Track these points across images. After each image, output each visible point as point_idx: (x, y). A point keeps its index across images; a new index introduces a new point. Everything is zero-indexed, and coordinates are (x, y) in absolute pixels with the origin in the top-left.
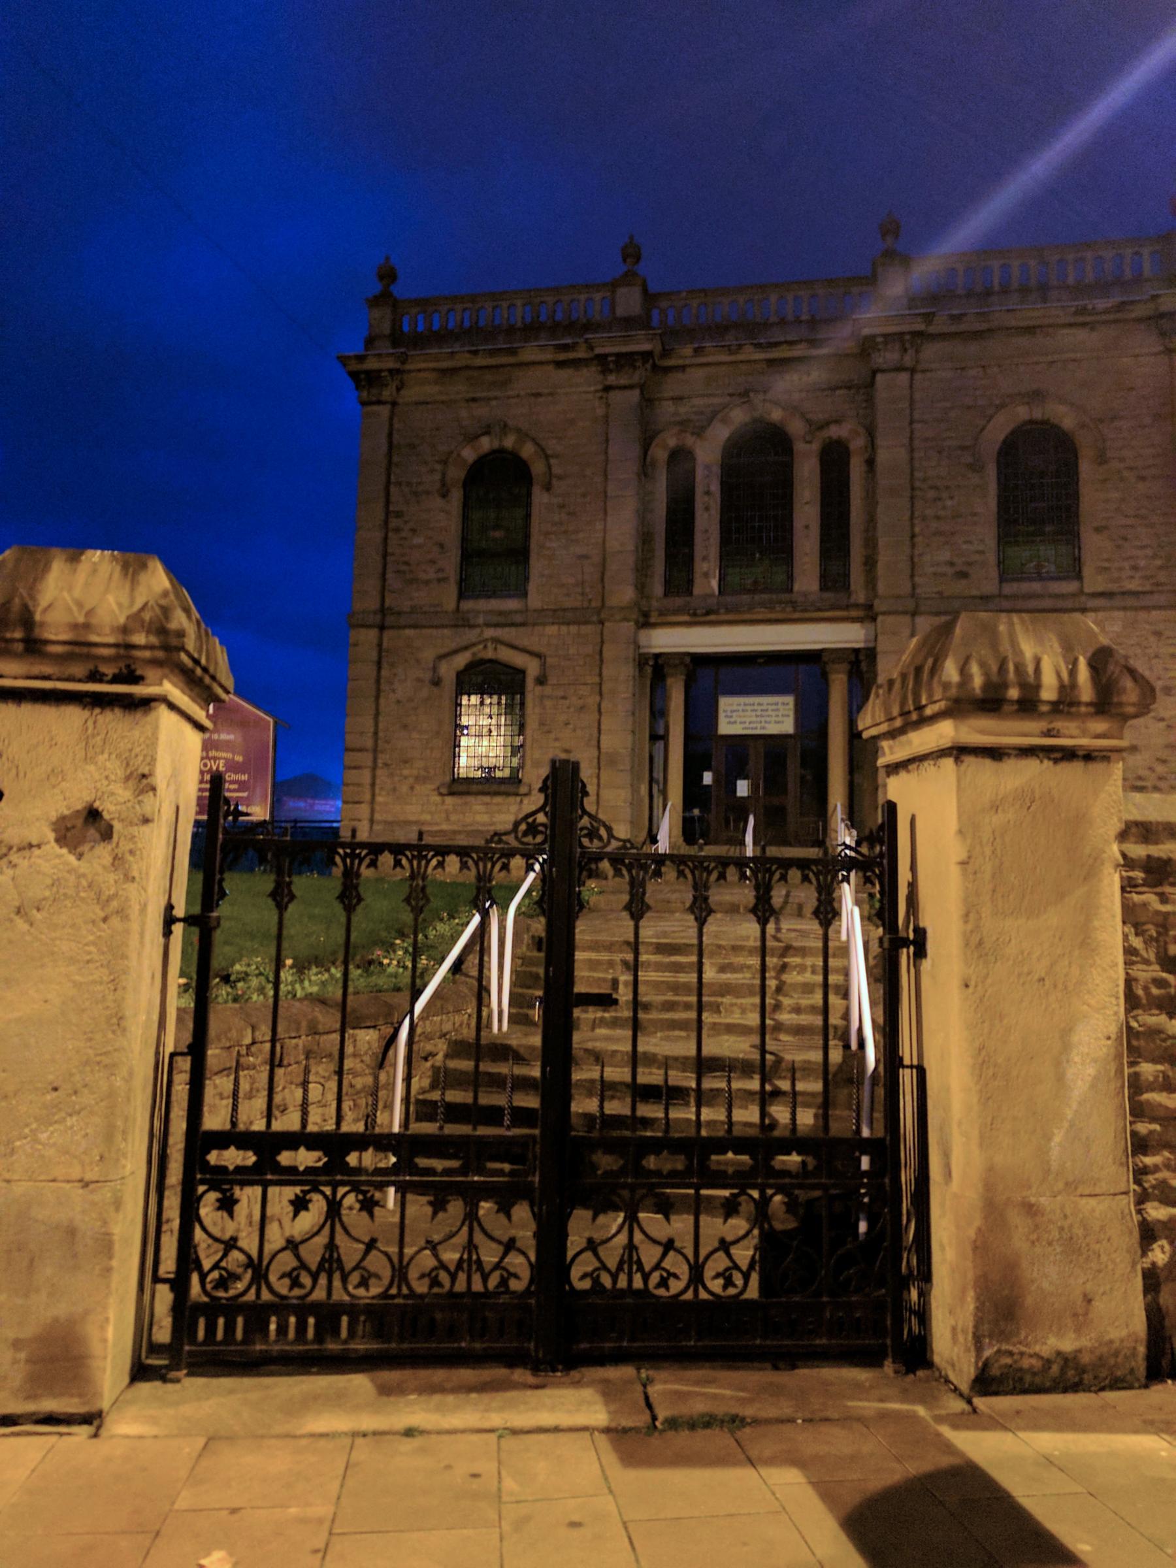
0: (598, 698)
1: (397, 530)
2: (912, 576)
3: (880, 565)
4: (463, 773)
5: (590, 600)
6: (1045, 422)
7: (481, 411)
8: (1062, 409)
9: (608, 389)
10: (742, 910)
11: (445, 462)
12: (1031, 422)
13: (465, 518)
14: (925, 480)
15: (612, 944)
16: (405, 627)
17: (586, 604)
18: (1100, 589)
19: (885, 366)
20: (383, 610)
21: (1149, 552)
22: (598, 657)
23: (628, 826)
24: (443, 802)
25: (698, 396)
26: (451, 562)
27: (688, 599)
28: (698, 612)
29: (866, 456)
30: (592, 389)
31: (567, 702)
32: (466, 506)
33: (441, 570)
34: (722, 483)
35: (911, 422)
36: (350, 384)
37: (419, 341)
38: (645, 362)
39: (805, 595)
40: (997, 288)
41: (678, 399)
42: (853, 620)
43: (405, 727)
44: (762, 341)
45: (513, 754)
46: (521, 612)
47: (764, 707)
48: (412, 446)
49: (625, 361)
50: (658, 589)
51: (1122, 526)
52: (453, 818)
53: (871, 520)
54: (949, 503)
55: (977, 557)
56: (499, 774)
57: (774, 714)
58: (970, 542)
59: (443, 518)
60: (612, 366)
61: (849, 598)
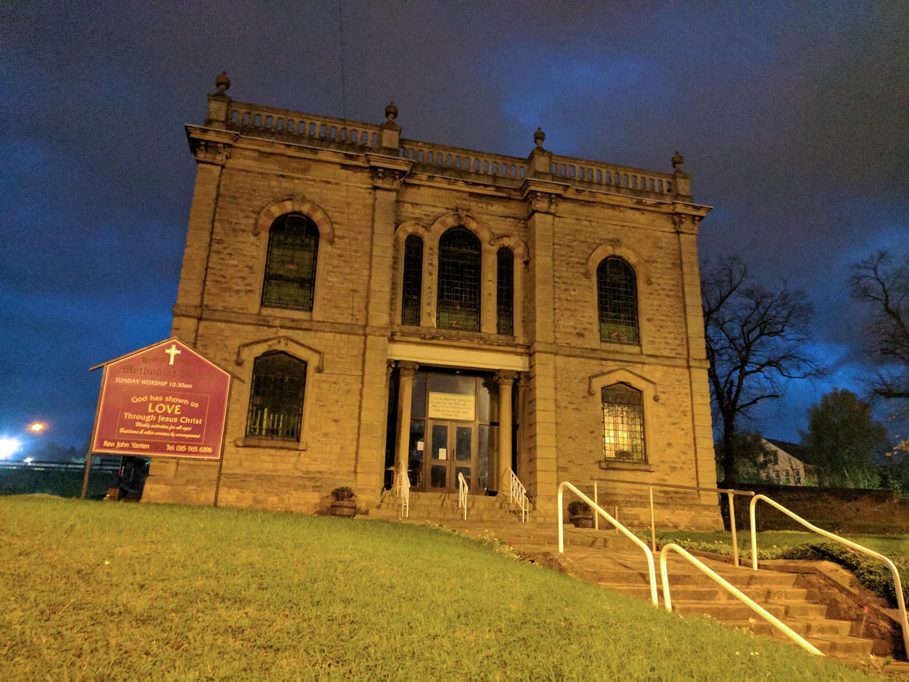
7: (286, 184)
8: (630, 252)
9: (375, 188)
13: (269, 252)
16: (218, 321)
17: (354, 322)
21: (673, 335)
24: (238, 451)
25: (427, 205)
30: (365, 186)
31: (338, 386)
34: (440, 260)
37: (246, 130)
39: (489, 335)
41: (414, 204)
42: (520, 354)
48: (235, 198)
49: (391, 174)
50: (398, 319)
52: (246, 464)
54: (573, 293)
55: (588, 326)
59: (254, 250)
60: (380, 175)
61: (514, 340)
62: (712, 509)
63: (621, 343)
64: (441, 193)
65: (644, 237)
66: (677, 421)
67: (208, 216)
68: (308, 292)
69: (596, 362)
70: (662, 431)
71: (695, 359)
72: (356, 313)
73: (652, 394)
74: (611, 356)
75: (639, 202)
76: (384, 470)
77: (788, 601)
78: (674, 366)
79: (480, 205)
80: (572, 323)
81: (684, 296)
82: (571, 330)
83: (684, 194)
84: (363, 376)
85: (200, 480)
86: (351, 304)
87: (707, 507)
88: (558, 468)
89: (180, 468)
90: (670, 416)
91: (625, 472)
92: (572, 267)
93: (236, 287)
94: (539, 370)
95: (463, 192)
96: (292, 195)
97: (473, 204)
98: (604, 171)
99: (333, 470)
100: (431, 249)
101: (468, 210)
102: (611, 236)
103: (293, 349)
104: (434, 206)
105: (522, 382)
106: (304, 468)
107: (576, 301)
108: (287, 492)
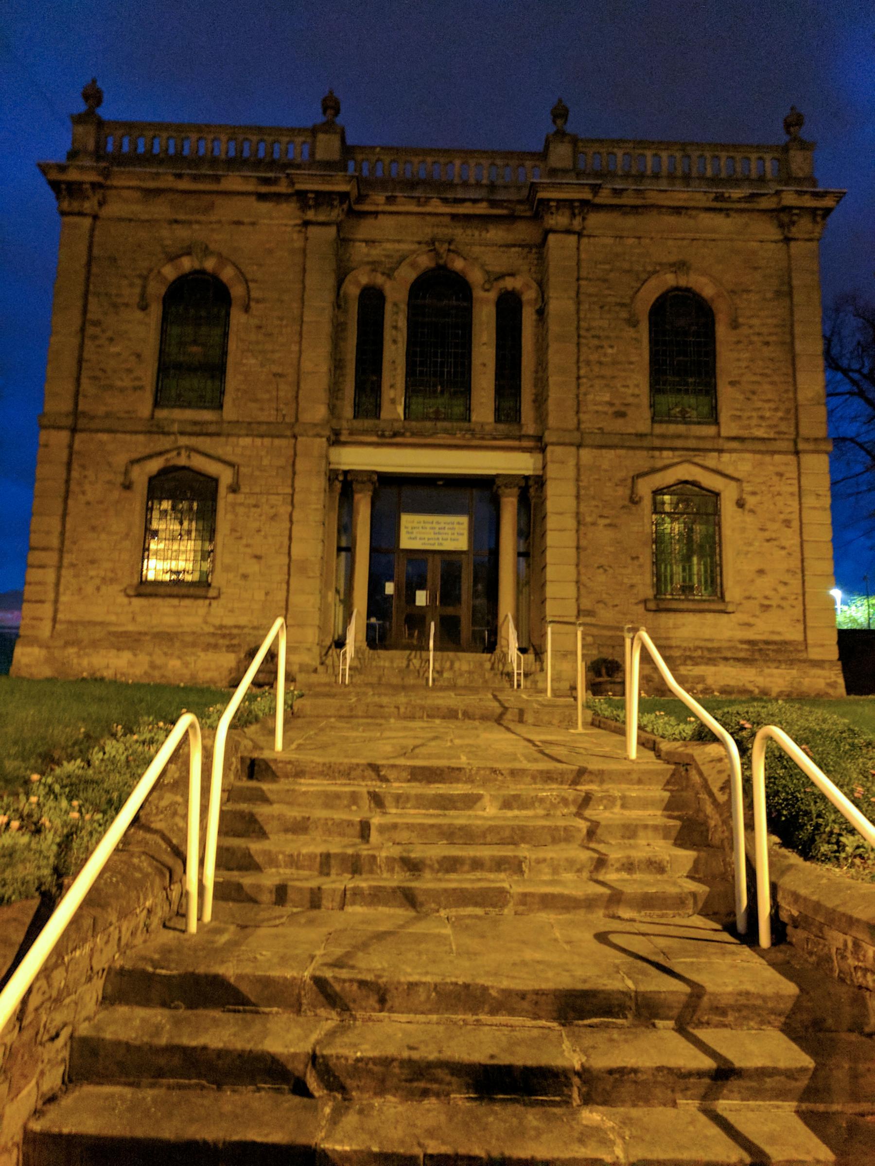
0: (289, 508)
1: (95, 338)
2: (578, 412)
3: (550, 401)
4: (151, 576)
5: (284, 416)
6: (688, 290)
7: (183, 233)
8: (704, 280)
9: (306, 223)
10: (460, 716)
11: (145, 278)
12: (677, 288)
13: (163, 332)
14: (588, 330)
15: (353, 768)
16: (98, 431)
17: (280, 419)
18: (734, 433)
19: (557, 228)
20: (76, 413)
21: (772, 405)
22: (290, 469)
23: (317, 631)
24: (130, 603)
25: (388, 241)
26: (148, 373)
27: (377, 422)
28: (387, 433)
29: (537, 307)
30: (292, 222)
31: (259, 510)
32: (165, 319)
33: (138, 379)
35: (578, 279)
36: (51, 194)
37: (121, 160)
38: (342, 203)
39: (482, 425)
40: (649, 172)
43: (93, 529)
44: (449, 196)
45: (203, 559)
46: (217, 423)
47: (442, 525)
49: (323, 199)
50: (348, 411)
51: (753, 382)
52: (140, 619)
53: (542, 365)
54: (610, 351)
55: (630, 400)
56: (189, 578)
57: (450, 532)
58: (627, 386)
59: (142, 331)
61: (520, 429)
62: (827, 665)
63: (686, 423)
64: (411, 219)
65: (721, 251)
66: (774, 536)
67: (79, 290)
68: (217, 383)
69: (645, 453)
70: (747, 553)
71: (807, 440)
72: (281, 406)
73: (735, 496)
74: (668, 443)
75: (719, 198)
76: (365, 622)
77: (627, 813)
78: (773, 453)
79: (469, 232)
80: (607, 398)
81: (792, 343)
82: (606, 409)
83: (801, 175)
84: (293, 495)
85: (82, 641)
86: (274, 393)
87: (818, 664)
88: (579, 611)
89: (58, 626)
90: (762, 529)
91: (686, 615)
92: (609, 311)
93: (119, 383)
94: (552, 471)
95: (442, 214)
96: (190, 247)
97: (459, 233)
98: (664, 155)
99: (256, 624)
100: (395, 304)
101: (450, 242)
102: (673, 258)
103: (199, 463)
104: (399, 241)
105: (532, 491)
106: (217, 622)
107: (615, 363)
108: (194, 654)
